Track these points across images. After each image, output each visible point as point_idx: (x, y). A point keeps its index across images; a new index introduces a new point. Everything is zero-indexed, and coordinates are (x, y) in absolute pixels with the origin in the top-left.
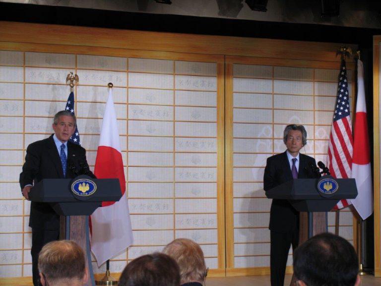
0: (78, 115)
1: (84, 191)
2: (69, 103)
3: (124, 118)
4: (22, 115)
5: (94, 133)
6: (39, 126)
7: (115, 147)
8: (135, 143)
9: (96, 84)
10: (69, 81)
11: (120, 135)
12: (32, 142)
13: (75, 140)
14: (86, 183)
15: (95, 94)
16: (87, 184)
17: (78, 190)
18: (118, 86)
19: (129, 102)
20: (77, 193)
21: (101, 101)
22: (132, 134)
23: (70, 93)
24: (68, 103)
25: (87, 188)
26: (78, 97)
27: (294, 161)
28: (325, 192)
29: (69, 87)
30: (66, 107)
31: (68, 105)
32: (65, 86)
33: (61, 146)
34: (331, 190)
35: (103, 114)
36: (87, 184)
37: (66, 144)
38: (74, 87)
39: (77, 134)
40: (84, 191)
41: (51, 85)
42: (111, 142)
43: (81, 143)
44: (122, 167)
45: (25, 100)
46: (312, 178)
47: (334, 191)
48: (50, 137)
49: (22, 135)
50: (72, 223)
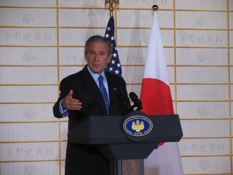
0: (118, 43)
1: (138, 130)
2: (109, 29)
3: (171, 45)
4: (56, 45)
5: (137, 64)
6: (74, 57)
7: (161, 79)
8: (184, 75)
9: (138, 7)
10: (108, 4)
11: (167, 66)
12: (69, 75)
13: (117, 72)
14: (140, 121)
15: (137, 19)
16: (142, 122)
17: (131, 129)
18: (164, 8)
19: (177, 27)
20: (130, 133)
21: (145, 27)
22: (180, 64)
23: (109, 18)
24: (107, 30)
25: (142, 127)
26: (118, 23)
27: (101, 78)
28: (133, 134)
29: (108, 11)
30: (106, 34)
31: (107, 32)
32: (104, 10)
33: (99, 79)
34: (142, 131)
35: (147, 41)
36: (142, 122)
37: (103, 74)
38: (114, 12)
39: (119, 65)
40: (138, 130)
41: (88, 10)
42: (158, 73)
43: (123, 75)
44: (171, 101)
45: (58, 28)
46: (142, 112)
47: (147, 133)
48: (84, 69)
49: (56, 68)
50: (124, 168)
